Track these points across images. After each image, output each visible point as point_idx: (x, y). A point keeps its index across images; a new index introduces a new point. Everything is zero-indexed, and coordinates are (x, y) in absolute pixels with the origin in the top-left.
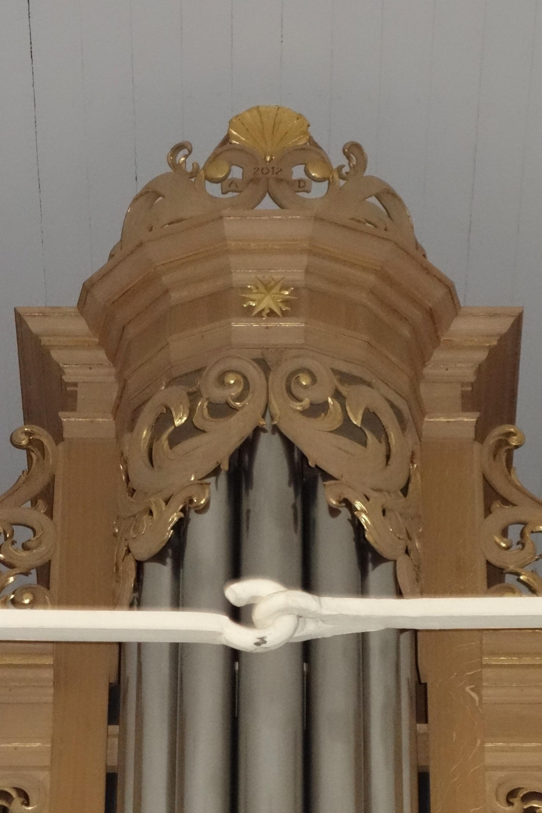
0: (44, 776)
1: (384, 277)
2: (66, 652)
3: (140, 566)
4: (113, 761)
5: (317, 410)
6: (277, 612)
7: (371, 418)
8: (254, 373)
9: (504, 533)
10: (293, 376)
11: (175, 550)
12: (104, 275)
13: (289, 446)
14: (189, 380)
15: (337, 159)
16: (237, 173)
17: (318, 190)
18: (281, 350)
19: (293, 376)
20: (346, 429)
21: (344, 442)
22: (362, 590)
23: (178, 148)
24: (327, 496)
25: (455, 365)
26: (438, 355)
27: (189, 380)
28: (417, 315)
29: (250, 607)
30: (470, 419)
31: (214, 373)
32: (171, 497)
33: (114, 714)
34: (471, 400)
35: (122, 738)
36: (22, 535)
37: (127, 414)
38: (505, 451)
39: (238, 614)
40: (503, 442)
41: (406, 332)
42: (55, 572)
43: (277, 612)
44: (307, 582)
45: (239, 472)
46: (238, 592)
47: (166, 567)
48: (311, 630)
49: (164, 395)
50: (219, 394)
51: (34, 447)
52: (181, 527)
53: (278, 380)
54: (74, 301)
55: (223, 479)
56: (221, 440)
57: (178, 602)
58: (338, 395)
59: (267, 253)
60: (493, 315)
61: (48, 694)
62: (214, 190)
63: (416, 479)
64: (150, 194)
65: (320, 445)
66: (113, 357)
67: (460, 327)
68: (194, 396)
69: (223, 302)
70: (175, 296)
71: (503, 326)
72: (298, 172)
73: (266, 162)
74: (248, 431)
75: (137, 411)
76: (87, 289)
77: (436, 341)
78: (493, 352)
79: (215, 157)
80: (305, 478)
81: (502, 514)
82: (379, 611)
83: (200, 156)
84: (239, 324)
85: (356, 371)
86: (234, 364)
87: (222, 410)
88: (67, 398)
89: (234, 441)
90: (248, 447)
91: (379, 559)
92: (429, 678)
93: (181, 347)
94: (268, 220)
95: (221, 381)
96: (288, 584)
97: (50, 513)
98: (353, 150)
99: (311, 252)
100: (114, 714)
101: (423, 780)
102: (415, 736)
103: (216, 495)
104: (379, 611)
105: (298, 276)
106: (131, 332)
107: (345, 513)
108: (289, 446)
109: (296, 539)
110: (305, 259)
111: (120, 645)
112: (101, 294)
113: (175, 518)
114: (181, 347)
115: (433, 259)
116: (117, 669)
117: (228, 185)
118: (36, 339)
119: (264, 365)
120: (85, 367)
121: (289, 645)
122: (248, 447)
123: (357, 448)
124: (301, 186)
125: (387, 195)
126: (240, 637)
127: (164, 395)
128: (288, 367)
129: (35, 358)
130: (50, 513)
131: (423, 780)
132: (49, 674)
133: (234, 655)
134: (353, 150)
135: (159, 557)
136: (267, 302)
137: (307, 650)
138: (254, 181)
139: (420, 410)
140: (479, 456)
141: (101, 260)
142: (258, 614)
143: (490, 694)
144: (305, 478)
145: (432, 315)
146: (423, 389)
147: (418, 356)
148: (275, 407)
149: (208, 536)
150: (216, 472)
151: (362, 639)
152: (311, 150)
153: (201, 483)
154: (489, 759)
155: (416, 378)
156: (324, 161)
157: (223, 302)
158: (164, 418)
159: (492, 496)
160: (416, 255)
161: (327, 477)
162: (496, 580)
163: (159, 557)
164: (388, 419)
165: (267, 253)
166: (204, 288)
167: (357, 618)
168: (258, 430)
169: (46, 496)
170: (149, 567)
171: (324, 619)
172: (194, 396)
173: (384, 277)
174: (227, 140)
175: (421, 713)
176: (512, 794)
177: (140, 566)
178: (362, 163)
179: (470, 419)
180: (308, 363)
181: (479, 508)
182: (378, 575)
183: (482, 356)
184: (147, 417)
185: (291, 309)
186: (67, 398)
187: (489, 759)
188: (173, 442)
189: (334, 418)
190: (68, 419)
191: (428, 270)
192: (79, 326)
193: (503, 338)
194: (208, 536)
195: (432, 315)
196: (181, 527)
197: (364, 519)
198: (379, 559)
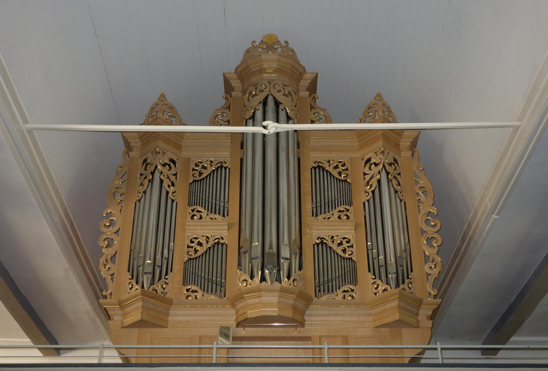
0: (229, 159)
1: (292, 66)
2: (233, 134)
3: (246, 120)
4: (242, 156)
5: (279, 91)
6: (272, 127)
7: (289, 93)
8: (268, 84)
9: (314, 114)
10: (275, 84)
11: (253, 117)
12: (239, 66)
13: (274, 98)
14: (255, 85)
15: (283, 44)
16: (264, 47)
17: (280, 50)
18: (273, 80)
19: (275, 84)
20: (285, 95)
21: (284, 97)
22: (288, 123)
23: (253, 42)
24: (281, 107)
25: (305, 83)
26: (302, 81)
27: (255, 85)
28: (298, 74)
29: (267, 126)
30: (308, 93)
31: (260, 84)
32: (126, 327)
33: (242, 148)
34: (308, 90)
35: (243, 151)
36: (225, 115)
37: (244, 92)
38: (314, 99)
39: (265, 127)
40: (314, 97)
41: (296, 77)
42: (231, 121)
43: (272, 127)
44: (277, 121)
45: (265, 103)
46: (265, 123)
47: (252, 120)
48: (278, 130)
49: (251, 88)
50: (261, 88)
51: (226, 98)
52: (254, 113)
53: (272, 85)
54: (234, 71)
55: (262, 104)
56: (262, 97)
57: (253, 126)
58: (283, 88)
59: (270, 61)
60: (312, 73)
61: (229, 144)
62: (260, 50)
63: (298, 104)
64: (248, 51)
65: (280, 97)
66: (241, 82)
67: (306, 76)
68: (256, 89)
69: (262, 71)
70: (253, 70)
71: (314, 75)
72: (276, 46)
73: (270, 44)
74: (266, 95)
75: (246, 91)
76: (236, 69)
77: (302, 79)
78: (312, 80)
79: (260, 44)
80: (277, 104)
81: (314, 111)
82: (291, 127)
83: (257, 44)
84: (265, 75)
85: (287, 84)
86: (264, 82)
87: (262, 91)
88: (233, 89)
89: (264, 97)
90: (267, 98)
91: (291, 119)
92: (300, 140)
93: (254, 79)
94: (271, 55)
95: (261, 85)
96: (274, 122)
97: (229, 111)
98: (286, 42)
99: (278, 61)
100: (242, 148)
101: (299, 160)
102: (297, 152)
103: (261, 107)
104: (291, 127)
105: (276, 66)
106: (245, 77)
107: (285, 110)
108: (274, 98)
109: (276, 115)
110: (277, 63)
111: (243, 133)
112: (239, 70)
113: (253, 111)
114: (254, 79)
115: (301, 63)
116: (241, 140)
117: (263, 49)
118: (227, 78)
119: (270, 83)
120: (236, 83)
121: (274, 133)
122: (267, 98)
123: (287, 98)
124: (276, 49)
125: (292, 51)
126: (265, 132)
127: (251, 88)
128: (274, 83)
129: (227, 82)
130: (229, 111)
131: (299, 160)
132: (230, 140)
133: (264, 135)
134: (286, 42)
135: (250, 119)
136: (270, 71)
137: (278, 134)
138: (267, 48)
139: (298, 91)
140: (309, 99)
141: (239, 63)
142: (269, 127)
143: (311, 144)
144: (277, 104)
145: (301, 73)
146: (299, 87)
147: (298, 81)
148: (271, 91)
149: (259, 114)
150: (260, 103)
151: (288, 132)
152: (278, 42)
153: (258, 105)
154: (311, 156)
155: (298, 85)
156: (281, 44)
157: (262, 71)
158: (251, 93)
159: (312, 107)
160: (298, 62)
161: (281, 103)
162: (312, 122)
163: (250, 119)
164: (292, 93)
165: (270, 61)
166: (259, 68)
167: (287, 128)
168: (268, 95)
169: (229, 107)
170: (248, 120)
171: (281, 128)
172: (256, 89)
173: (292, 66)
174: (262, 40)
175: (298, 147)
176: (315, 162)
177: (246, 120)
178: (288, 44)
179: (308, 93)
180: (278, 82)
181: (309, 109)
182: (290, 122)
183: (310, 81)
184: (248, 92)
185: (274, 72)
186: (233, 89)
187: (311, 156)
188: (253, 97)
189: (282, 93)
190: (233, 93)
191: (300, 65)
192: (235, 76)
193: (314, 78)
194: (259, 114)
195: (301, 73)
196: (254, 113)
197: (288, 111)
198: (291, 119)
